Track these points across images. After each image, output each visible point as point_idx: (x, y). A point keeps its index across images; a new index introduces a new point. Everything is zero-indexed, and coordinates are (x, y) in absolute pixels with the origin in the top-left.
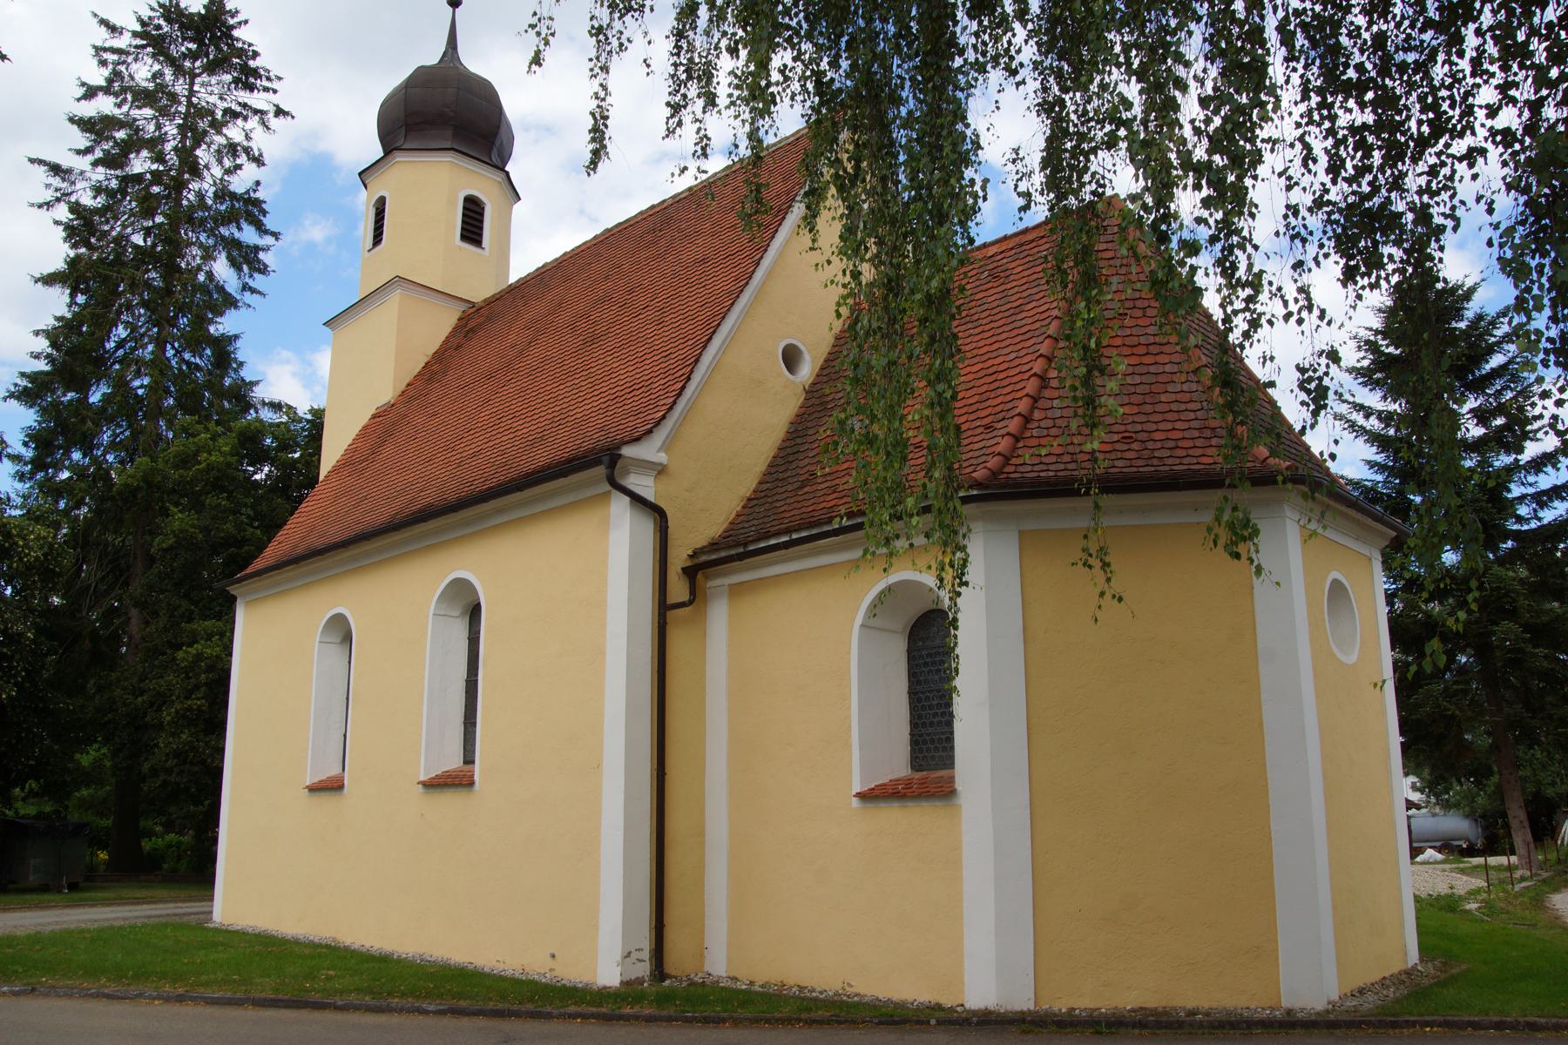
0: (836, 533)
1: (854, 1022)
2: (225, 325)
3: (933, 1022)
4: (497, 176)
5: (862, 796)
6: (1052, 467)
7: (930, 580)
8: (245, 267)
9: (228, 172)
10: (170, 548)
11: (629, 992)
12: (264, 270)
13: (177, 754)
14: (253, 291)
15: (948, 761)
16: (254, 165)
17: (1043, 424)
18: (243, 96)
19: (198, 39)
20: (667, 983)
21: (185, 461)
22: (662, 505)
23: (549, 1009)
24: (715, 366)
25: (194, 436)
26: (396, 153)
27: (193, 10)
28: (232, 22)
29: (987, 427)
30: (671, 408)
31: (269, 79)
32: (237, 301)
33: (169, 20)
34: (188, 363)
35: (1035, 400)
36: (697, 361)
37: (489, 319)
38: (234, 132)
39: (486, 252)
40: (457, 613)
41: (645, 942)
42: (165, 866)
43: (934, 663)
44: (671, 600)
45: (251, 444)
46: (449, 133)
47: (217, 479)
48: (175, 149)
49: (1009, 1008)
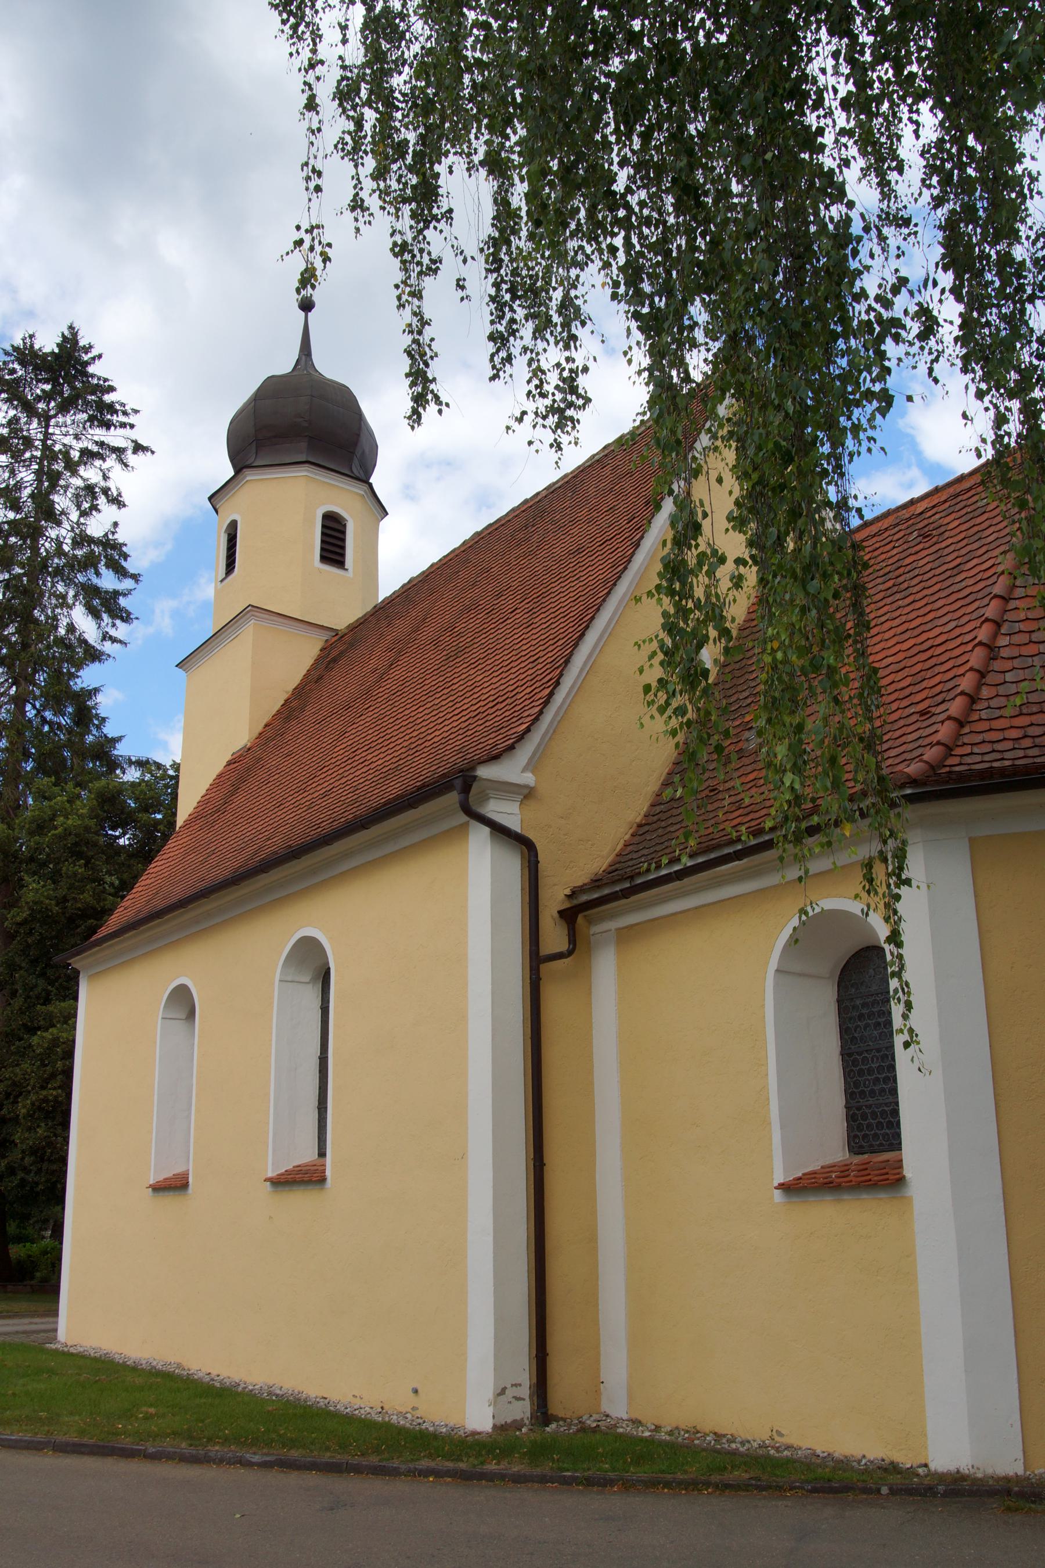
0: (738, 856)
1: (779, 1488)
2: (88, 677)
3: (885, 1490)
4: (359, 489)
5: (786, 1188)
6: (1007, 755)
7: (855, 907)
8: (105, 616)
9: (84, 514)
10: (25, 922)
11: (501, 1442)
12: (126, 617)
13: (34, 1151)
14: (114, 640)
15: (894, 1142)
16: (114, 507)
17: (994, 703)
18: (98, 433)
19: (53, 380)
20: (553, 1426)
21: (40, 827)
22: (531, 835)
23: (395, 1463)
24: (591, 668)
25: (49, 799)
26: (247, 472)
27: (47, 350)
28: (86, 358)
29: (922, 713)
30: (537, 719)
31: (125, 413)
32: (102, 653)
33: (23, 364)
34: (51, 723)
35: (982, 675)
36: (567, 662)
37: (351, 645)
38: (91, 474)
39: (350, 574)
40: (307, 978)
41: (523, 1375)
42: (38, 1274)
43: (871, 1015)
44: (546, 949)
45: (112, 807)
46: (304, 445)
47: (76, 844)
48: (32, 496)
49: (990, 1471)
